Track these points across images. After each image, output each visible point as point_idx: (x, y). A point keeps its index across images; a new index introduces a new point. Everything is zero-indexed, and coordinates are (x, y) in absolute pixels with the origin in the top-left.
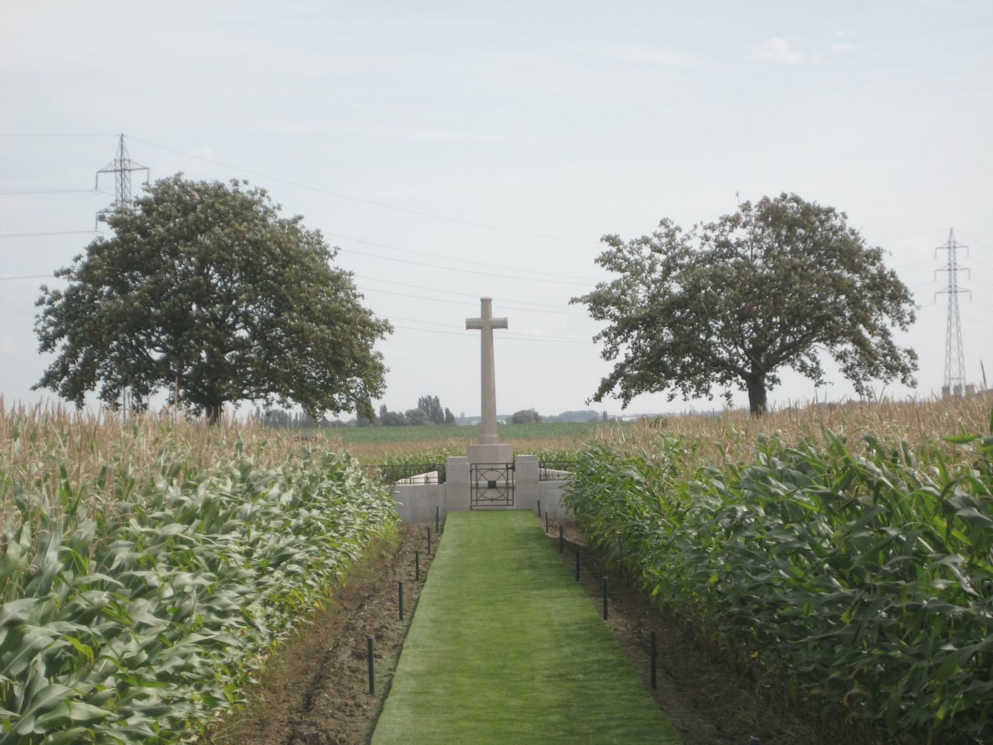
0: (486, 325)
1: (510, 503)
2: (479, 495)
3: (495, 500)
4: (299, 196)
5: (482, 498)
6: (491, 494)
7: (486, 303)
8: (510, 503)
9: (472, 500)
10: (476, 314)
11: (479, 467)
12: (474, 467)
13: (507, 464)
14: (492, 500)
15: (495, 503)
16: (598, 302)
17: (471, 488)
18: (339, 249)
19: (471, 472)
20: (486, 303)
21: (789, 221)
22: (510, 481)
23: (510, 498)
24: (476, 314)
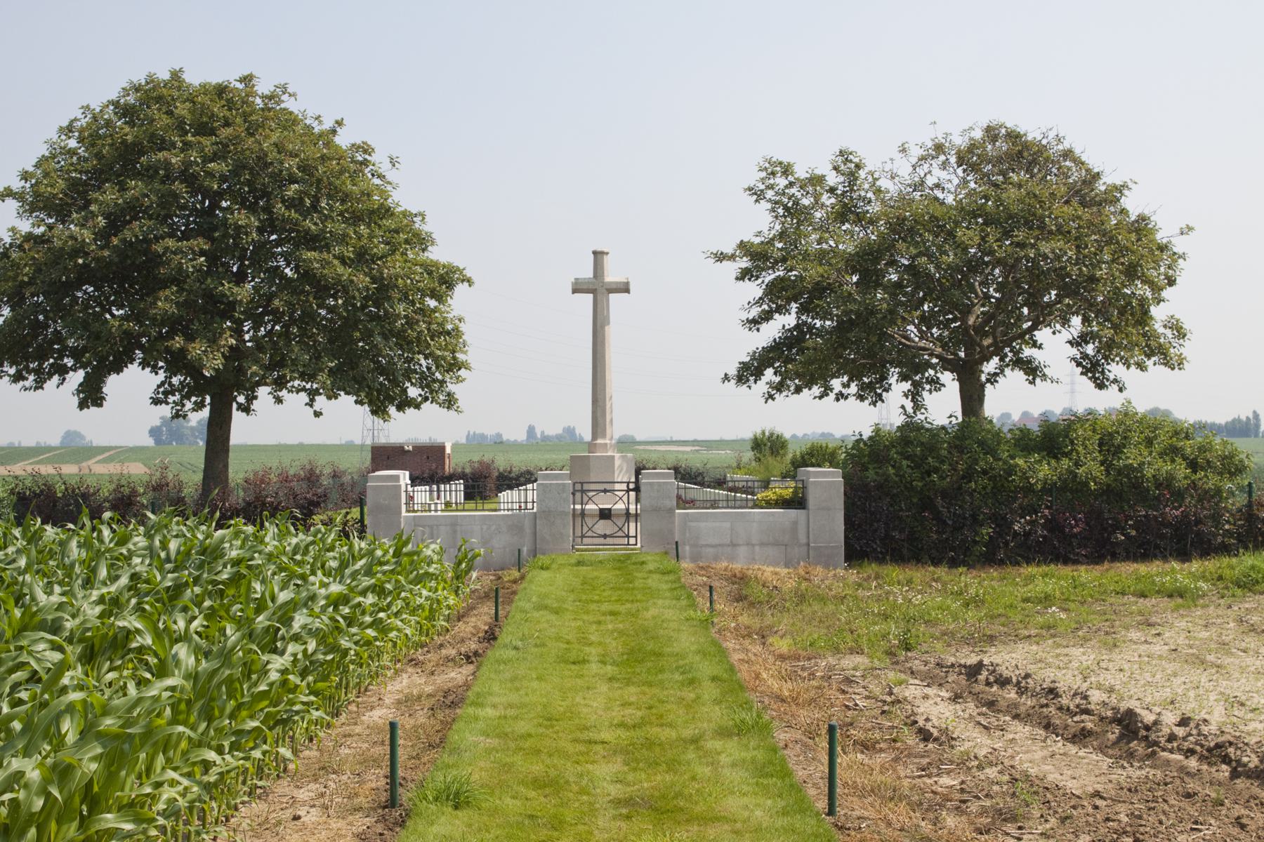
0: (597, 288)
1: (632, 541)
2: (585, 529)
3: (611, 536)
4: (331, 89)
5: (590, 534)
6: (603, 527)
7: (625, 288)
8: (632, 541)
9: (582, 483)
10: (587, 272)
11: (586, 487)
12: (578, 487)
13: (628, 483)
14: (605, 536)
15: (609, 540)
16: (757, 258)
17: (574, 515)
18: (602, 253)
19: (573, 494)
20: (625, 288)
21: (1008, 157)
22: (632, 507)
23: (632, 533)
24: (587, 272)
